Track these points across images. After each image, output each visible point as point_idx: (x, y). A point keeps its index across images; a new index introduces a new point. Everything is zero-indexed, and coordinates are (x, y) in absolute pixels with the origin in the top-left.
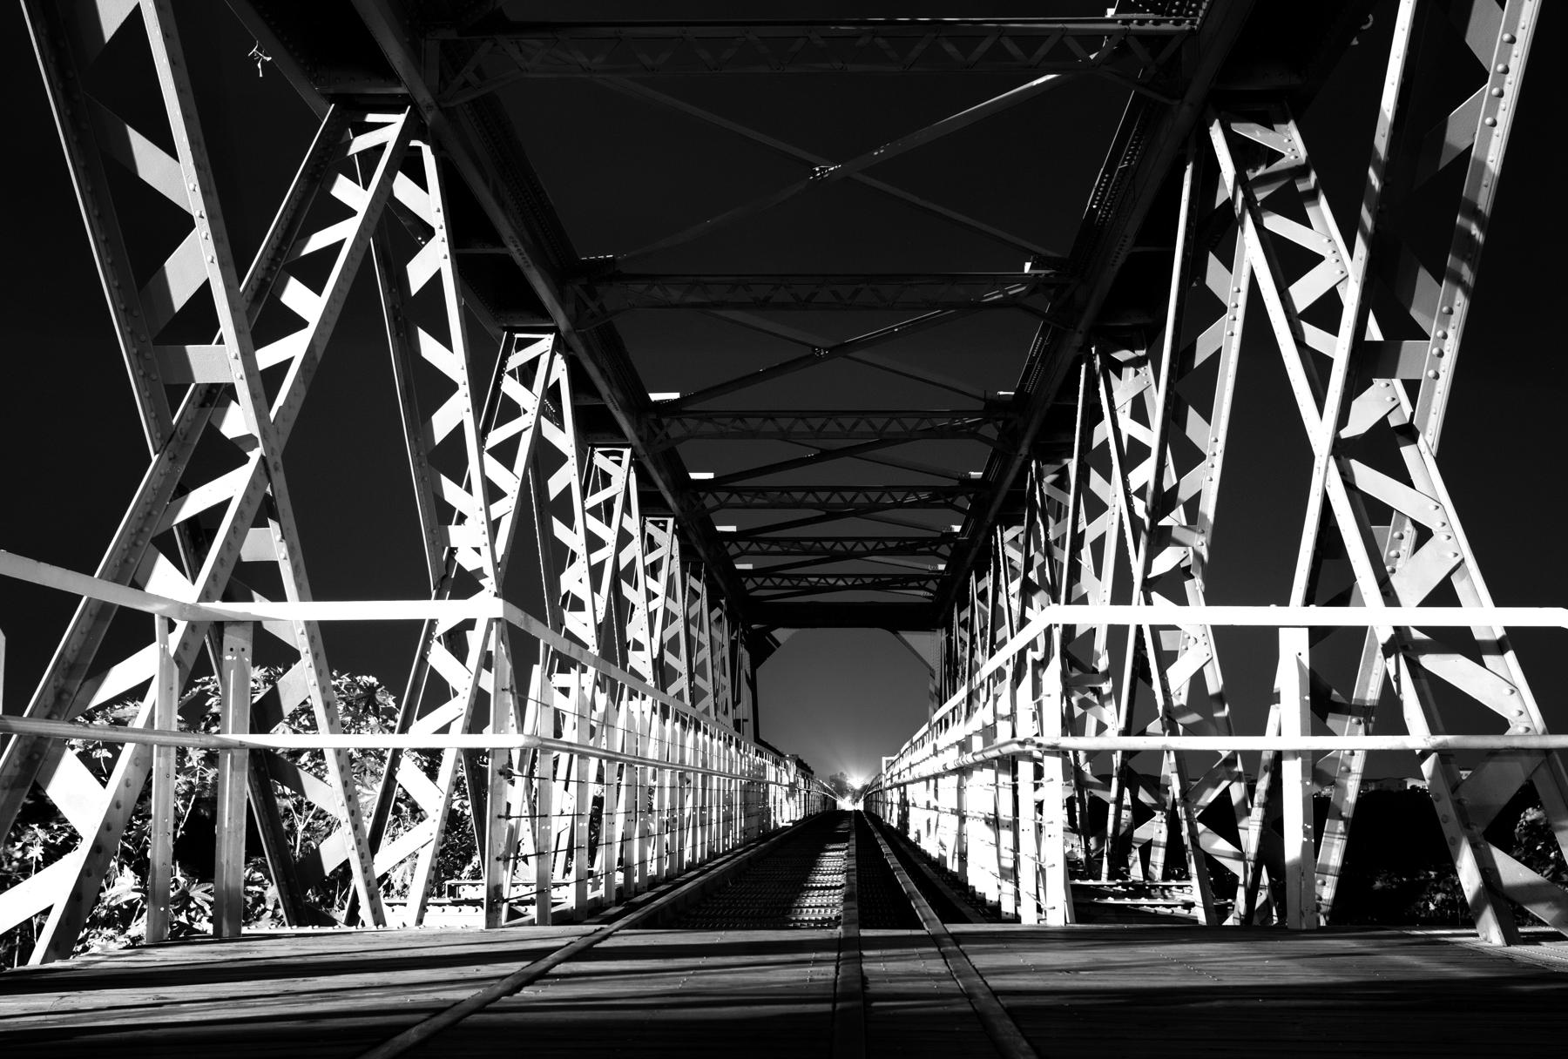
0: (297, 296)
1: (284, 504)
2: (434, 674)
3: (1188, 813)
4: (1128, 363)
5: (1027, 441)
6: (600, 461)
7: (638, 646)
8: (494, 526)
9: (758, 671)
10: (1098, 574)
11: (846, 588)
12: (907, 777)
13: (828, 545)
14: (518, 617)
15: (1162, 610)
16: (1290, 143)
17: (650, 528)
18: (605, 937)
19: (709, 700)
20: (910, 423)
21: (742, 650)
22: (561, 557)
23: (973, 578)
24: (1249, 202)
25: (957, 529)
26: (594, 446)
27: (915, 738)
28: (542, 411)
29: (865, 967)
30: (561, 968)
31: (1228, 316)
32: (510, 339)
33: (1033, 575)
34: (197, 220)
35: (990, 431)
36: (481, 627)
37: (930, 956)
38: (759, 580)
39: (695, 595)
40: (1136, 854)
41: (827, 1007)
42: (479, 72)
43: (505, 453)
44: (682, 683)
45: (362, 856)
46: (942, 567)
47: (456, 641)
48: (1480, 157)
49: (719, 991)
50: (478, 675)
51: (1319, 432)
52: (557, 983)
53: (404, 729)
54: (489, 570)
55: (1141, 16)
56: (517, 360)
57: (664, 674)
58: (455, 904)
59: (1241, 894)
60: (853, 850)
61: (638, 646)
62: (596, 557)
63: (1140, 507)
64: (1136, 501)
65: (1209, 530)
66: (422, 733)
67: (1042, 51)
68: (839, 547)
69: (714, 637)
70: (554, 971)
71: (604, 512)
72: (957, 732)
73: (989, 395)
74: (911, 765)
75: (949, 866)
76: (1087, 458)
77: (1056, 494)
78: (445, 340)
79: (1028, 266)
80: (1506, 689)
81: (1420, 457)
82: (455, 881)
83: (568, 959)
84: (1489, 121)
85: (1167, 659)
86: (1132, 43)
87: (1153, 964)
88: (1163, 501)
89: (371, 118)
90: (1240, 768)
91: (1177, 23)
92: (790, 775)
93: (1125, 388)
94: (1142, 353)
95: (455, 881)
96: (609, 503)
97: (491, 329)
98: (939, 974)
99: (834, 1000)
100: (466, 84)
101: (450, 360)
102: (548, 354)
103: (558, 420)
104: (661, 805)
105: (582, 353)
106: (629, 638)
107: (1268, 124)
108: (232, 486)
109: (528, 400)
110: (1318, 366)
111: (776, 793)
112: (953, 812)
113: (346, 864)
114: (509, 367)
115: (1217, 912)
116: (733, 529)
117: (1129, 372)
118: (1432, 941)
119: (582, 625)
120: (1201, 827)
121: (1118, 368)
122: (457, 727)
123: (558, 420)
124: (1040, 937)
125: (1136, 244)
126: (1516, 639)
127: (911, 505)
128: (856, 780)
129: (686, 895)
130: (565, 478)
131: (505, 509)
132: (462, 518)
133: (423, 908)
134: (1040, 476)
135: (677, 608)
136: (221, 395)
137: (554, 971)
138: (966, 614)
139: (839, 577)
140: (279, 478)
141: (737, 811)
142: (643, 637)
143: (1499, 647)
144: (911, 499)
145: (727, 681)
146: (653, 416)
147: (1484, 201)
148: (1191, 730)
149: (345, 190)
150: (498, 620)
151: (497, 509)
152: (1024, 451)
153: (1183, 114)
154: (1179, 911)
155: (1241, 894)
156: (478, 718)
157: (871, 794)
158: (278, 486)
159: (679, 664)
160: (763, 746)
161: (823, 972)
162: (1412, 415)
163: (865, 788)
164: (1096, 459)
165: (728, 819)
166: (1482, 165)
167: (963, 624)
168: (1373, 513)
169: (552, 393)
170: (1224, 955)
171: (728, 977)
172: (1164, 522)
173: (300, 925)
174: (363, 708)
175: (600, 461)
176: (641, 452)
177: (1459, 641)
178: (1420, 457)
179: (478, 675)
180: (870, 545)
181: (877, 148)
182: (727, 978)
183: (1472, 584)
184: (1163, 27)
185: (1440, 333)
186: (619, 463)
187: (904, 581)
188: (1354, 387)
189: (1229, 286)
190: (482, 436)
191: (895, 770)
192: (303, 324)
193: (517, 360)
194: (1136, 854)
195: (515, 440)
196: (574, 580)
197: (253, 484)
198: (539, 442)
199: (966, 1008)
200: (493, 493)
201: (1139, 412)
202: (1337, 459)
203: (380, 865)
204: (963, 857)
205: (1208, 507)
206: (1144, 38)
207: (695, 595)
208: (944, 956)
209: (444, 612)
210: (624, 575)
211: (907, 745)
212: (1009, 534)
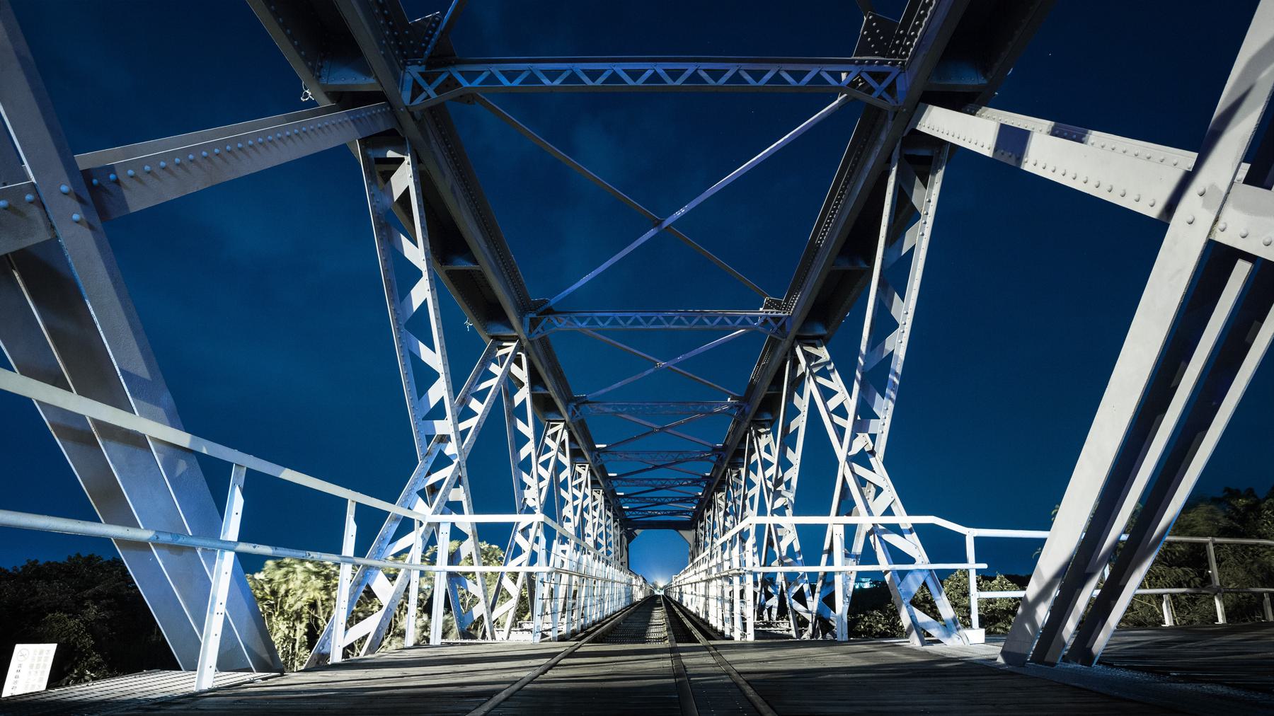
0: (475, 405)
1: (465, 480)
2: (517, 545)
3: (788, 595)
4: (764, 433)
5: (727, 462)
6: (578, 469)
7: (589, 536)
8: (541, 490)
9: (630, 545)
10: (752, 508)
11: (661, 515)
12: (683, 583)
13: (655, 500)
14: (549, 522)
15: (777, 519)
16: (823, 353)
17: (594, 493)
18: (579, 647)
19: (612, 555)
20: (686, 456)
21: (624, 537)
22: (563, 502)
23: (706, 511)
24: (811, 372)
25: (700, 494)
26: (576, 463)
27: (686, 569)
28: (558, 450)
29: (683, 660)
30: (563, 662)
31: (801, 415)
32: (548, 424)
33: (728, 510)
34: (441, 375)
35: (714, 458)
36: (534, 526)
37: (704, 656)
38: (631, 512)
39: (609, 517)
40: (766, 610)
41: (673, 680)
42: (542, 328)
43: (545, 464)
44: (603, 549)
45: (488, 613)
46: (694, 508)
47: (525, 532)
48: (897, 354)
49: (628, 673)
50: (532, 546)
51: (841, 453)
52: (562, 669)
53: (505, 565)
54: (538, 507)
55: (772, 310)
56: (551, 432)
57: (597, 545)
58: (521, 631)
59: (810, 625)
60: (665, 610)
61: (589, 536)
62: (575, 503)
63: (770, 485)
64: (768, 481)
65: (794, 492)
66: (512, 566)
67: (738, 321)
68: (659, 500)
69: (615, 533)
70: (560, 663)
71: (579, 487)
72: (704, 566)
73: (714, 446)
74: (684, 579)
75: (701, 616)
76: (749, 467)
77: (737, 480)
78: (526, 423)
79: (729, 399)
80: (914, 547)
81: (877, 462)
82: (521, 622)
83: (565, 657)
84: (900, 341)
85: (780, 539)
86: (769, 319)
87: (795, 658)
88: (778, 482)
89: (505, 344)
90: (806, 578)
91: (784, 313)
92: (641, 582)
93: (763, 441)
94: (768, 429)
95: (521, 622)
96: (580, 484)
97: (542, 421)
98: (712, 664)
99: (675, 677)
100: (538, 332)
101: (527, 430)
102: (561, 430)
103: (564, 454)
104: (597, 594)
105: (573, 429)
106: (586, 532)
107: (815, 346)
108: (447, 473)
109: (554, 445)
110: (840, 431)
111: (636, 589)
112: (703, 596)
113: (482, 616)
114: (548, 434)
115: (800, 633)
116: (623, 494)
117: (763, 436)
118: (894, 645)
119: (569, 528)
120: (793, 601)
121: (759, 435)
122: (525, 564)
123: (564, 454)
124: (743, 646)
125: (768, 390)
126: (917, 528)
127: (685, 485)
128: (661, 584)
129: (607, 630)
130: (566, 474)
131: (545, 484)
132: (529, 487)
133: (510, 633)
134: (731, 475)
135: (602, 522)
136: (444, 439)
137: (560, 663)
138: (703, 524)
139: (659, 511)
140: (464, 470)
141: (623, 596)
142: (590, 532)
143: (910, 531)
144: (685, 483)
145: (619, 548)
146: (597, 453)
147: (899, 369)
148: (789, 564)
149: (494, 368)
150: (542, 522)
151: (541, 485)
152: (725, 465)
153: (786, 344)
154: (785, 632)
155: (810, 625)
156: (533, 559)
157: (667, 589)
158: (464, 473)
159: (603, 542)
160: (632, 572)
161: (666, 663)
162: (873, 447)
163: (665, 587)
164: (752, 468)
165: (619, 599)
166: (898, 357)
167: (702, 528)
168: (862, 482)
169: (562, 444)
170: (820, 653)
171: (630, 666)
172: (778, 489)
173: (464, 639)
174: (487, 557)
175: (578, 469)
176: (592, 466)
177: (895, 529)
178: (877, 462)
179: (532, 546)
180: (670, 500)
181: (679, 356)
182: (629, 666)
183: (898, 507)
184: (779, 314)
185: (884, 417)
186: (584, 469)
187: (681, 512)
188: (854, 436)
189: (802, 404)
190: (538, 457)
191: (678, 580)
192: (477, 414)
193: (551, 432)
194: (766, 610)
195: (548, 460)
196: (567, 511)
197: (455, 472)
198: (557, 461)
199: (728, 681)
200: (541, 479)
201: (768, 449)
202: (848, 462)
203: (495, 616)
204: (707, 613)
205: (794, 484)
206: (773, 318)
207: (609, 517)
208: (712, 655)
209: (522, 520)
210: (585, 509)
211: (683, 571)
212: (719, 495)
